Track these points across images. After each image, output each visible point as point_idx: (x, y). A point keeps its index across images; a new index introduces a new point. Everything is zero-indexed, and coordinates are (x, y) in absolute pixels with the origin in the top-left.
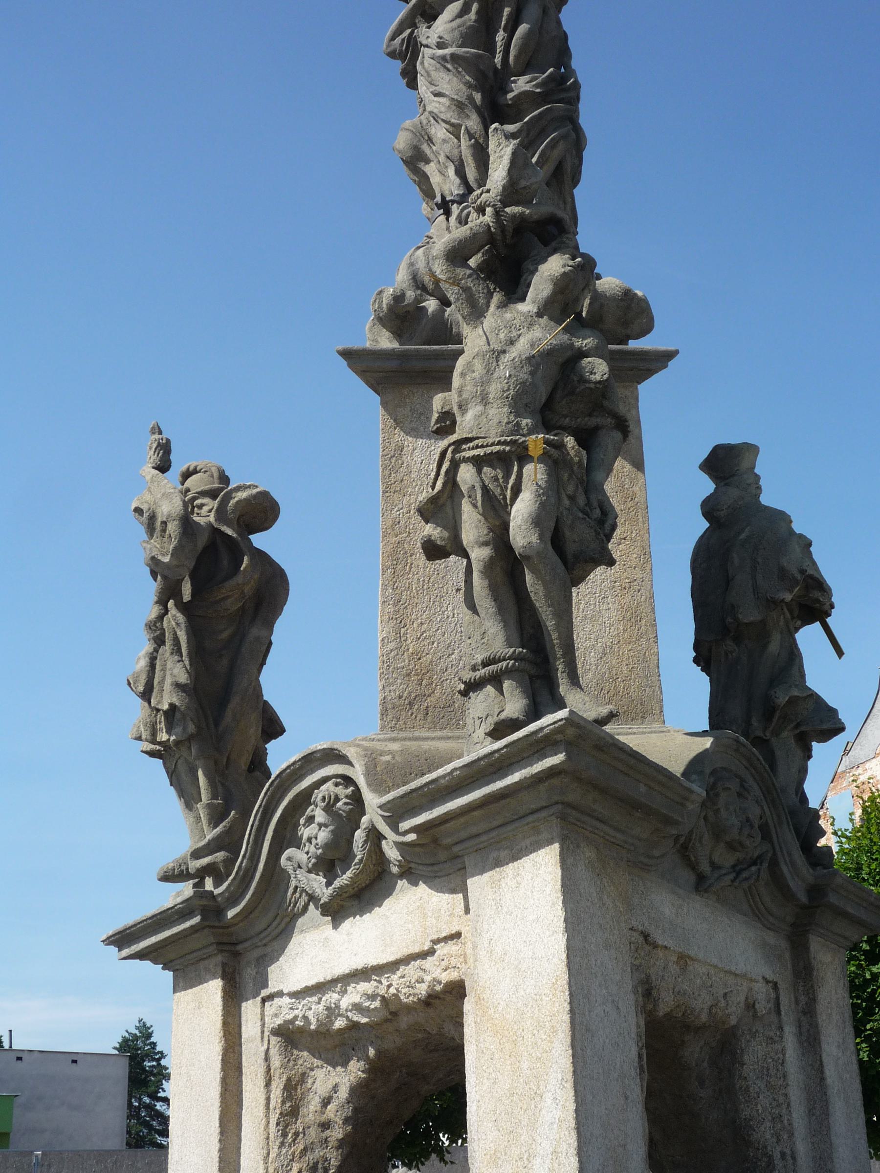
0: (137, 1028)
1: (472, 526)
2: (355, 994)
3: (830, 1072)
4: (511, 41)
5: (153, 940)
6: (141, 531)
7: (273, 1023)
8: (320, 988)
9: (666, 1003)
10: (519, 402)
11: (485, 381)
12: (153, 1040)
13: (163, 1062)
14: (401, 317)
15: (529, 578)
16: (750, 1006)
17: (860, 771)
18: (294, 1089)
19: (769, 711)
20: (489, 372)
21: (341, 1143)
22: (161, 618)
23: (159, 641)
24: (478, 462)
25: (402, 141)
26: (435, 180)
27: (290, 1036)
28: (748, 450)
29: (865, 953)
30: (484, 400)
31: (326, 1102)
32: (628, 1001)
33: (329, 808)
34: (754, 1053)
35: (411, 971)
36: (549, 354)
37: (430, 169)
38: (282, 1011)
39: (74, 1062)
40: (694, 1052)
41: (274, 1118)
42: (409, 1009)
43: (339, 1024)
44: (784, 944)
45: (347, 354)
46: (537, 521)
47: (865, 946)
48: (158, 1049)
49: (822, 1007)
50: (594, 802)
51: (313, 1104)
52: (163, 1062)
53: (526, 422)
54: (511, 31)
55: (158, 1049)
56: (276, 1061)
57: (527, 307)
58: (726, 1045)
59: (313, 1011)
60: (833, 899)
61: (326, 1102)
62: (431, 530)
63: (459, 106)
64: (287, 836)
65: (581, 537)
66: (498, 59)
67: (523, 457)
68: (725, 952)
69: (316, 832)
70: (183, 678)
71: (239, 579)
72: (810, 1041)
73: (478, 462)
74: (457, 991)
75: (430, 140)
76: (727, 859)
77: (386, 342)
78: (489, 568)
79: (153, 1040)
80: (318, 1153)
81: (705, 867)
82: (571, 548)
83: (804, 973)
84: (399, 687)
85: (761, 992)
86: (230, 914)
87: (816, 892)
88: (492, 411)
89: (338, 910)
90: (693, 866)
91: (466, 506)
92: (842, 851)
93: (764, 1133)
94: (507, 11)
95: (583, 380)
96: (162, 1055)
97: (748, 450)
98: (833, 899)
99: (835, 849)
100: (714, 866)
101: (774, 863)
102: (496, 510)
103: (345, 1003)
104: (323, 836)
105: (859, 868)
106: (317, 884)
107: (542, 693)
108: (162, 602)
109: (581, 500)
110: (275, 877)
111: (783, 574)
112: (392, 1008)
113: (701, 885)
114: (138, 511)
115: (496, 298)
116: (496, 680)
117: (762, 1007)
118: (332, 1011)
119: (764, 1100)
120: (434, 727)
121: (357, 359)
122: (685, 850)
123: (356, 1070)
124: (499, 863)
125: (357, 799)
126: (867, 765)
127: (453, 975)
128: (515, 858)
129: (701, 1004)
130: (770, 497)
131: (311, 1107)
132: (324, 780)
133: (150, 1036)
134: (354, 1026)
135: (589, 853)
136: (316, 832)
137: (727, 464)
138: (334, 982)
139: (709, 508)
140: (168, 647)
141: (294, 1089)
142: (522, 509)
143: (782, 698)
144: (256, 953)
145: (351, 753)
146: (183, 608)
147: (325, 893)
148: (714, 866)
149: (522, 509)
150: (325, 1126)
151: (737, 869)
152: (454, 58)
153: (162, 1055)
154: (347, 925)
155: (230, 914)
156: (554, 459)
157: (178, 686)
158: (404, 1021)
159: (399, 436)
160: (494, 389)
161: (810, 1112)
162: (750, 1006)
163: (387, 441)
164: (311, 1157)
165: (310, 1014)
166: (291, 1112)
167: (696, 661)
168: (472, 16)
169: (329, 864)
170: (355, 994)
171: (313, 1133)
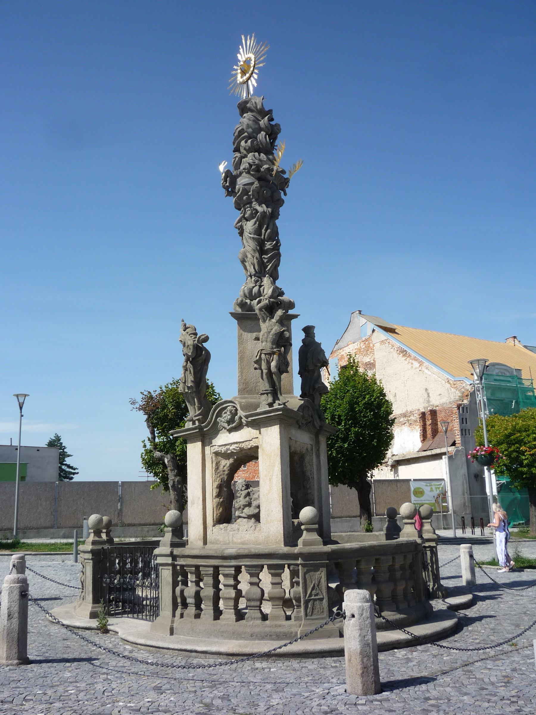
0: (55, 437)
1: (264, 366)
2: (233, 446)
3: (322, 462)
4: (266, 233)
5: (185, 433)
6: (181, 346)
7: (212, 451)
8: (226, 445)
9: (293, 449)
10: (273, 343)
11: (267, 338)
12: (61, 441)
13: (65, 450)
14: (242, 305)
15: (274, 376)
16: (307, 449)
17: (341, 350)
18: (217, 464)
19: (314, 389)
20: (268, 336)
21: (227, 474)
22: (186, 365)
23: (186, 370)
24: (265, 354)
25: (240, 256)
26: (248, 268)
27: (217, 454)
28: (313, 327)
29: (337, 422)
30: (267, 341)
31: (224, 466)
32: (288, 450)
33: (231, 412)
34: (307, 458)
35: (247, 443)
36: (360, 607)
37: (247, 264)
38: (216, 449)
39: (38, 450)
40: (296, 458)
41: (214, 470)
42: (245, 450)
43: (229, 452)
44: (314, 437)
45: (231, 313)
46: (276, 367)
47: (337, 420)
48: (63, 445)
49: (321, 449)
50: (286, 419)
51: (221, 467)
52: (65, 450)
53: (274, 346)
54: (266, 230)
55: (63, 445)
56: (214, 459)
57: (274, 320)
58: (302, 457)
59: (223, 449)
60: (324, 428)
61: (224, 466)
62: (256, 366)
63: (254, 251)
64: (219, 415)
65: (284, 366)
66: (262, 237)
67: (274, 353)
68: (304, 439)
69: (226, 416)
70: (193, 379)
71: (203, 356)
72: (318, 456)
73: (265, 354)
74: (257, 447)
75: (247, 257)
76: (304, 422)
77: (239, 310)
78: (267, 374)
79: (61, 441)
80: (223, 476)
81: (301, 424)
82: (281, 370)
83: (318, 443)
84: (242, 386)
85: (309, 446)
86: (205, 430)
87: (321, 427)
88: (268, 344)
89: (230, 431)
90: (298, 424)
91: (263, 362)
92: (331, 389)
93: (308, 473)
94: (265, 226)
95: (284, 337)
96: (65, 448)
97: (313, 327)
98: (324, 428)
99: (329, 388)
100: (302, 424)
101: (313, 422)
102: (269, 363)
103: (231, 448)
104: (229, 417)
105: (336, 395)
106: (226, 425)
107: (276, 398)
108: (187, 362)
109: (283, 361)
110: (216, 423)
111: (319, 360)
112: (242, 449)
113: (300, 427)
114: (181, 341)
115: (268, 318)
116: (267, 394)
117: (309, 449)
118: (228, 450)
119: (309, 467)
120: (249, 394)
121: (232, 314)
122: (297, 422)
123: (231, 460)
124: (267, 427)
125: (236, 410)
126: (344, 349)
127: (256, 445)
128: (271, 426)
129: (298, 450)
130: (317, 339)
131: (221, 467)
132: (229, 406)
133: (60, 440)
134: (232, 452)
135: (283, 425)
136: (226, 416)
137: (308, 331)
138: (229, 444)
139: (303, 341)
140: (188, 372)
141: (217, 464)
142: (273, 364)
143: (317, 387)
144: (208, 437)
145: (236, 402)
146: (191, 362)
147: (228, 428)
148: (302, 424)
149: (273, 364)
150: (224, 471)
151: (306, 424)
152: (253, 238)
153: (65, 448)
154: (232, 433)
155: (205, 430)
156: (280, 355)
157: (192, 381)
158: (243, 452)
159: (241, 331)
160: (269, 340)
161: (317, 470)
162: (307, 449)
163: (239, 333)
164: (221, 477)
165: (222, 450)
166: (217, 469)
167: (299, 374)
168: (257, 225)
169: (229, 422)
170: (233, 446)
171: (221, 473)
